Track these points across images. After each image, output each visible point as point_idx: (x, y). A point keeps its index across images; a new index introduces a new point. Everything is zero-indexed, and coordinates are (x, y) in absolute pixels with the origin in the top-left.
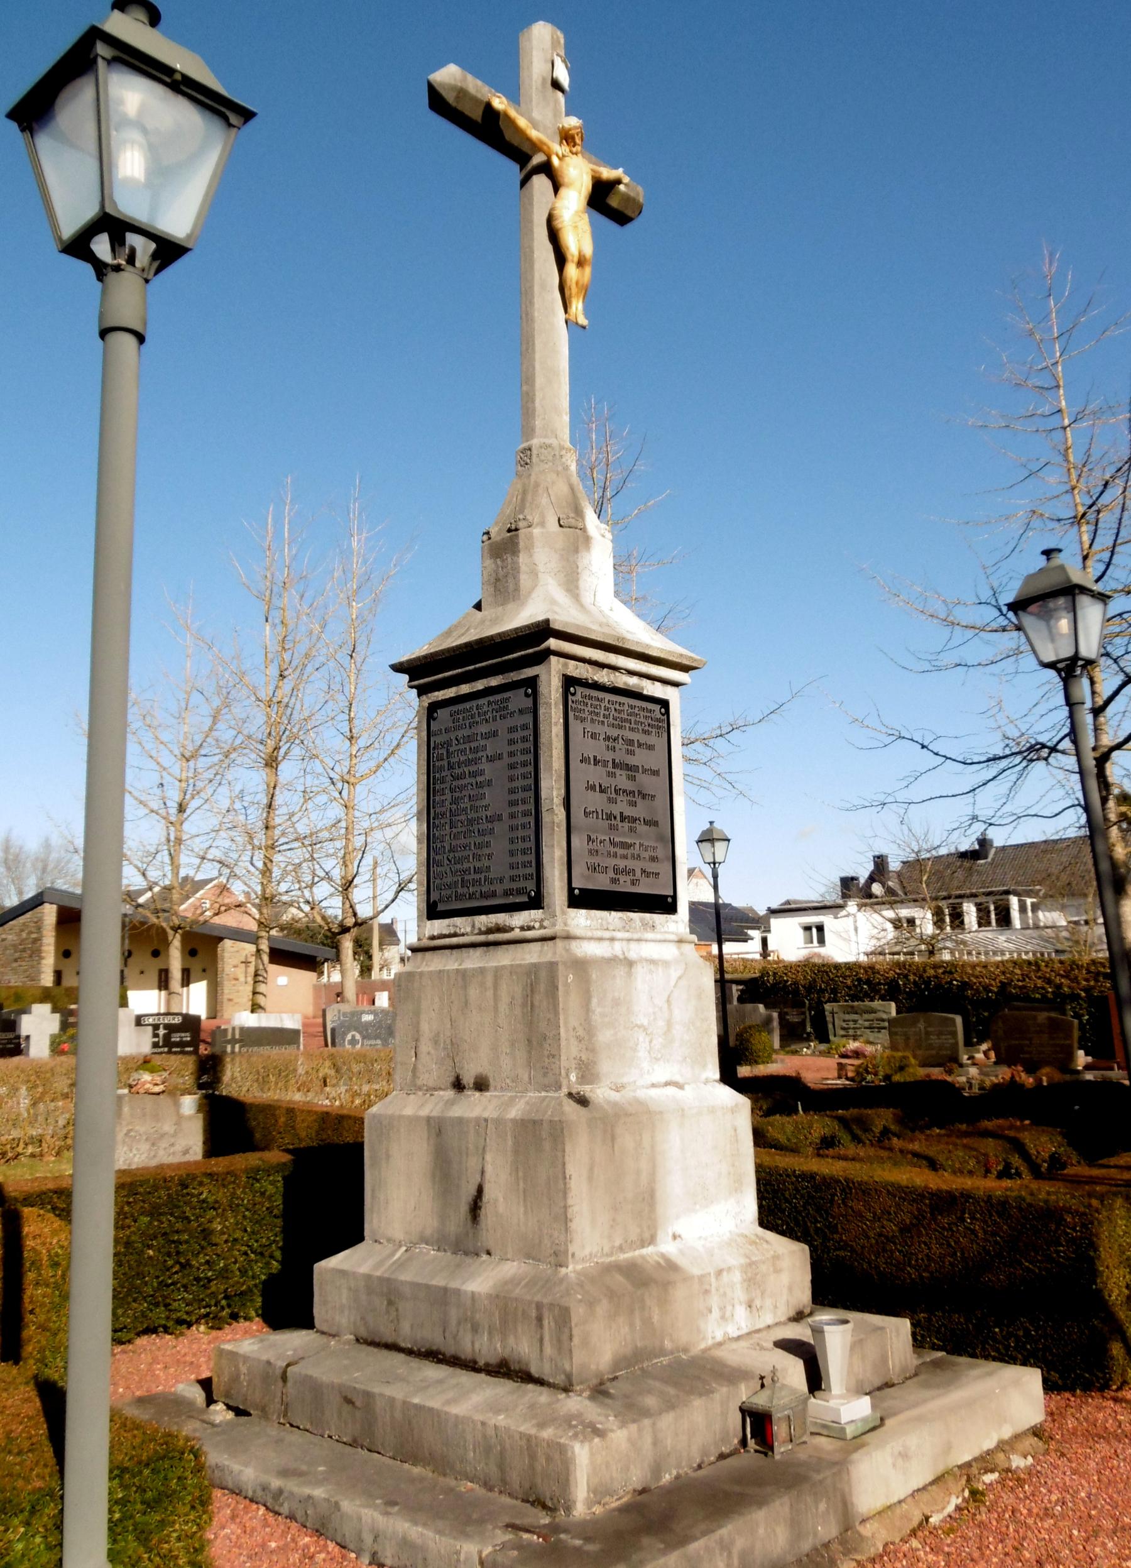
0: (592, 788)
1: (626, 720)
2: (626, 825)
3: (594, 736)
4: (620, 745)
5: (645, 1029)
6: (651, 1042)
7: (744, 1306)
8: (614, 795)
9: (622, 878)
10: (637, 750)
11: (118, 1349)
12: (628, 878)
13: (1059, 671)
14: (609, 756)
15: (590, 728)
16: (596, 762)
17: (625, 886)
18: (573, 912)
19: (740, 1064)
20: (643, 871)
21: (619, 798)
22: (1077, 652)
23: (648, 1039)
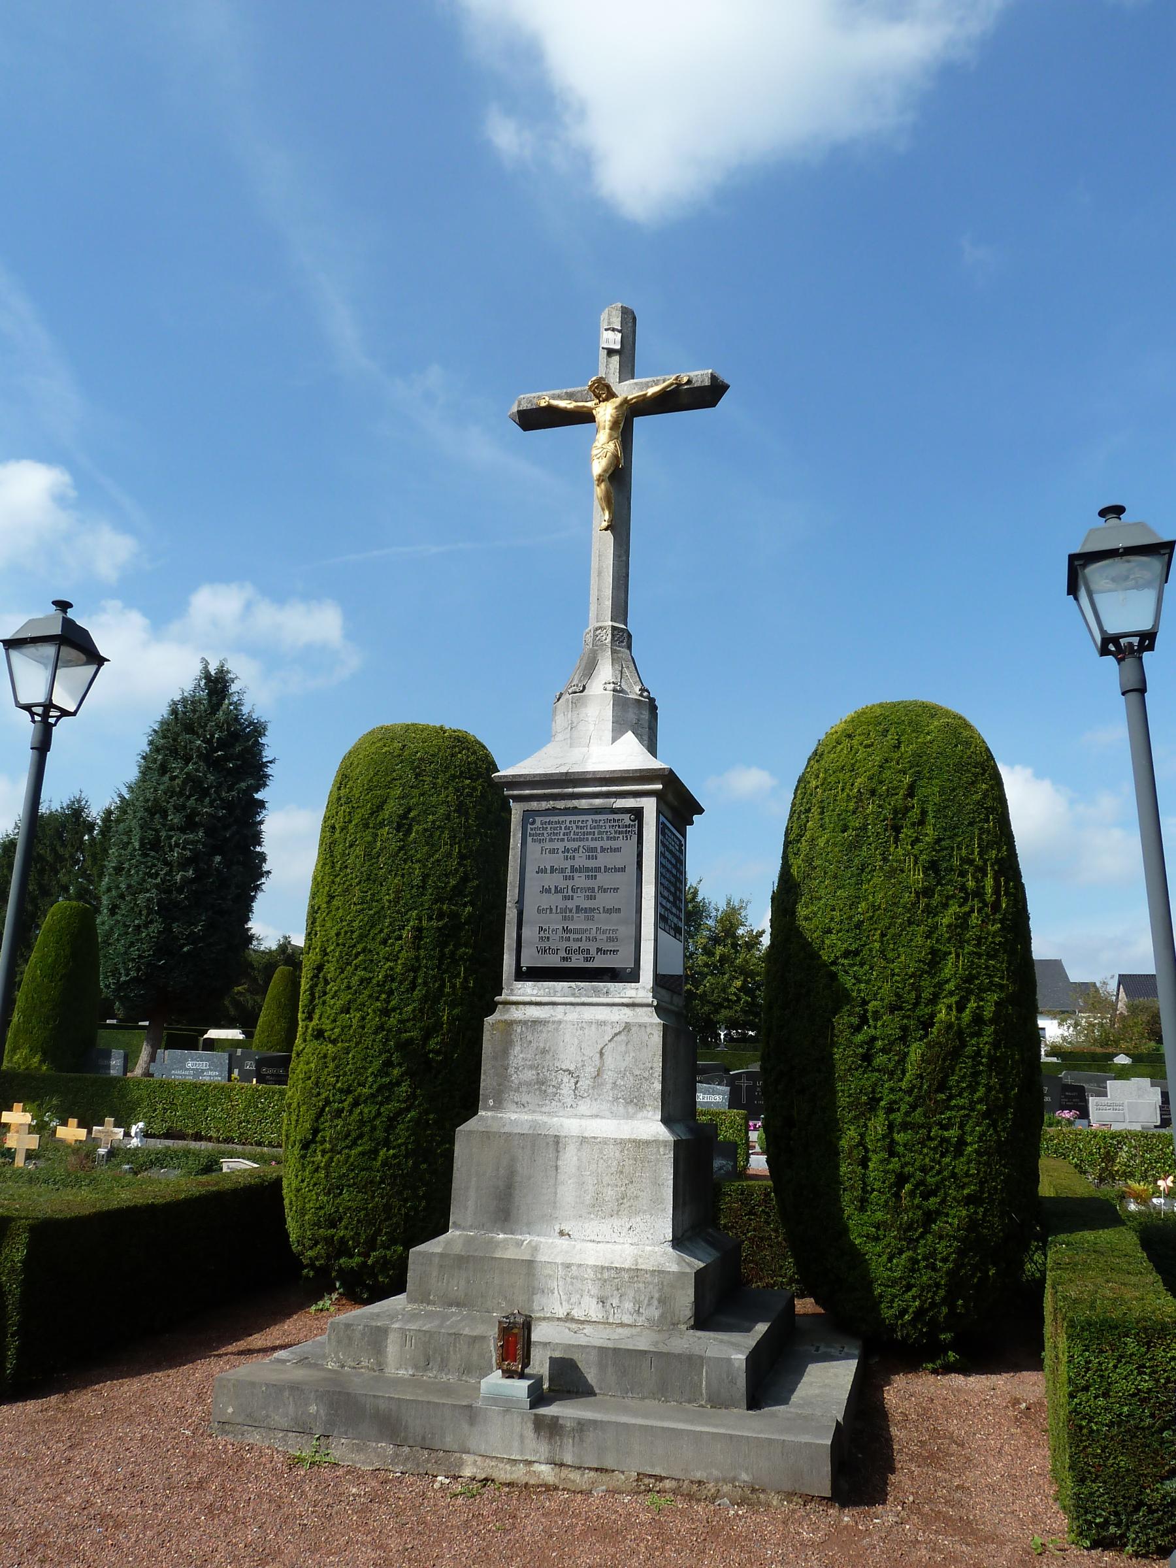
0: (548, 891)
1: (588, 833)
2: (582, 915)
3: (552, 851)
4: (582, 854)
5: (570, 1073)
6: (577, 1083)
7: (595, 1301)
8: (570, 893)
9: (574, 957)
10: (600, 855)
11: (905, 1479)
12: (581, 957)
13: (32, 714)
14: (568, 864)
15: (548, 845)
16: (553, 870)
17: (577, 962)
18: (519, 984)
19: (1037, 1192)
20: (599, 950)
21: (575, 895)
22: (51, 700)
23: (573, 1081)
